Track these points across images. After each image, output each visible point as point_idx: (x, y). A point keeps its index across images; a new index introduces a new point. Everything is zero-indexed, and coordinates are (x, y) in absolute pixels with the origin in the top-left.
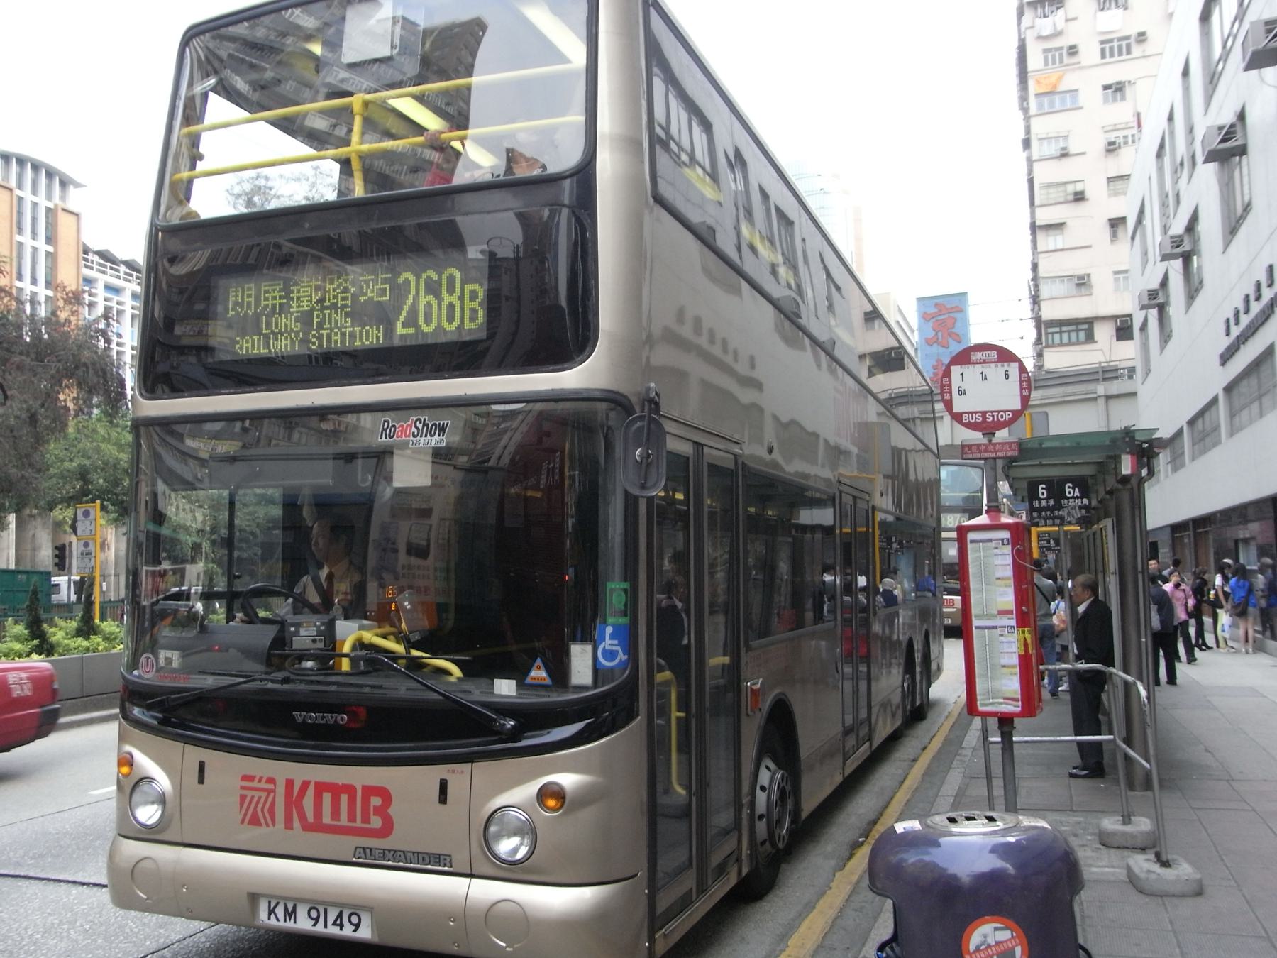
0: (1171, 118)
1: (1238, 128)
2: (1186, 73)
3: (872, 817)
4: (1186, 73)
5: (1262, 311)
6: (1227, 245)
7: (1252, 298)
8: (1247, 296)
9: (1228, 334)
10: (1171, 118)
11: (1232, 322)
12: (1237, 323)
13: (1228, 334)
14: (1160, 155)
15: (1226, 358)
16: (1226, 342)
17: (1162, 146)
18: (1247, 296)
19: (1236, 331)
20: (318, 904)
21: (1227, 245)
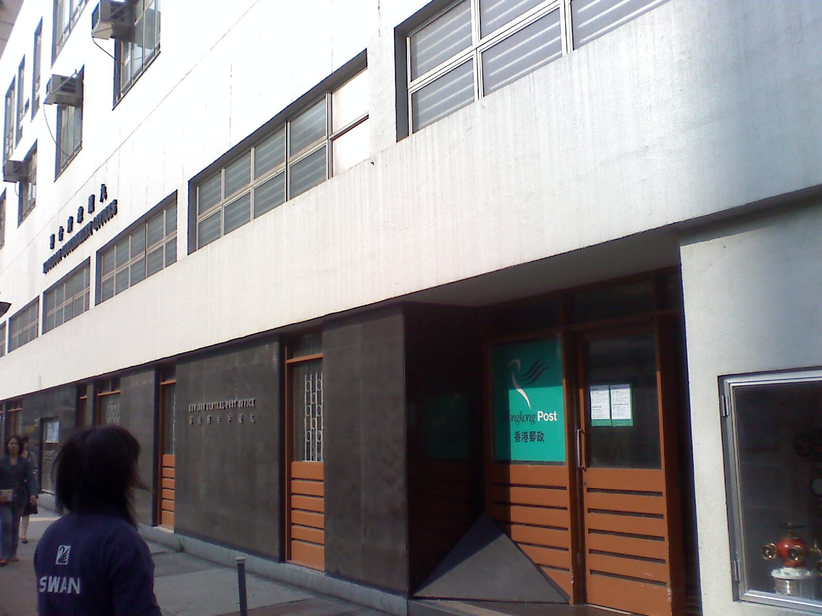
0: (22, 67)
1: (127, 14)
2: (38, 33)
3: (433, 129)
4: (38, 33)
5: (83, 231)
6: (19, 225)
7: (75, 220)
8: (72, 218)
9: (52, 247)
10: (22, 67)
11: (57, 238)
12: (61, 239)
13: (52, 247)
14: (8, 95)
15: (48, 266)
16: (49, 254)
17: (12, 87)
18: (72, 218)
19: (59, 245)
20: (734, 399)
21: (19, 225)
